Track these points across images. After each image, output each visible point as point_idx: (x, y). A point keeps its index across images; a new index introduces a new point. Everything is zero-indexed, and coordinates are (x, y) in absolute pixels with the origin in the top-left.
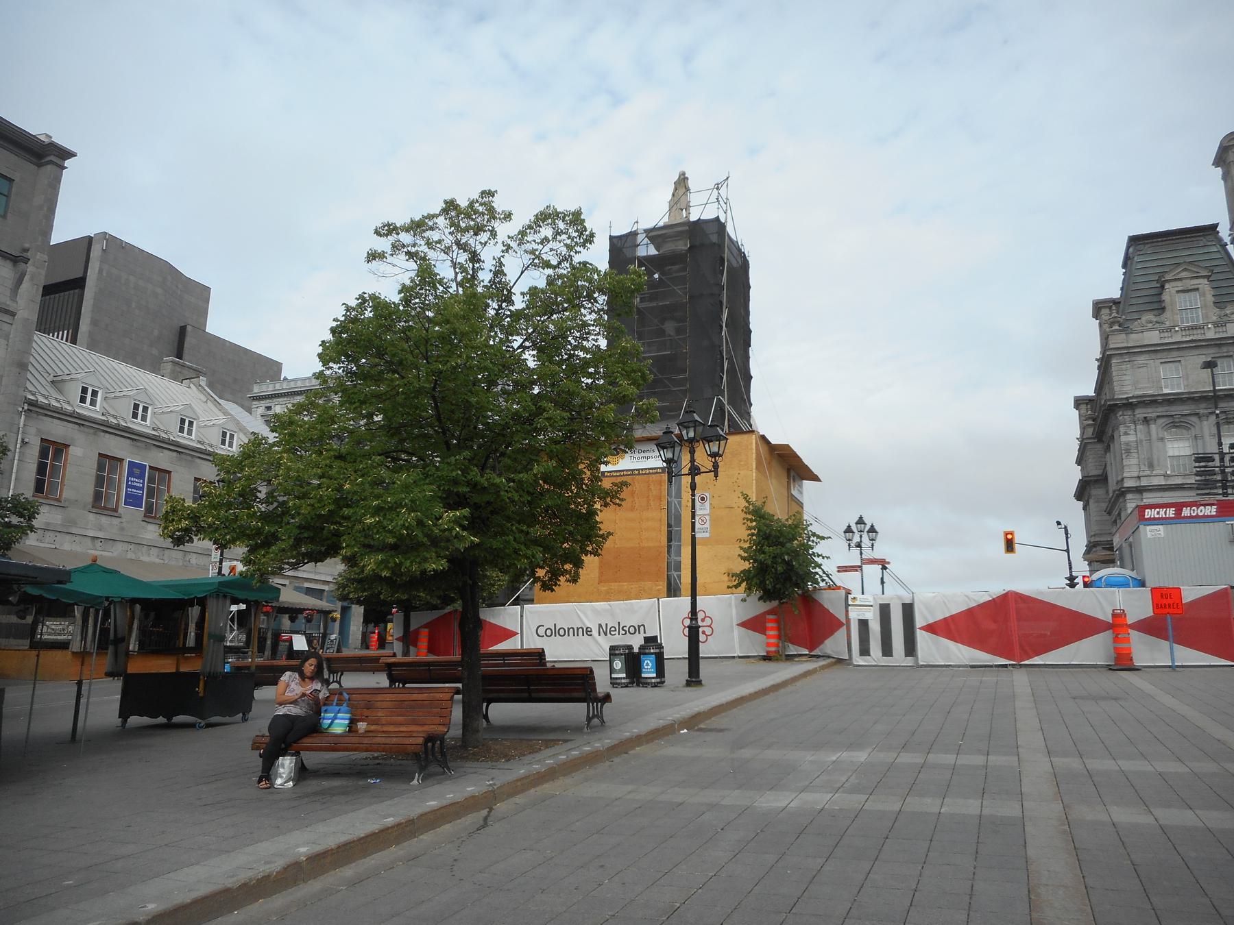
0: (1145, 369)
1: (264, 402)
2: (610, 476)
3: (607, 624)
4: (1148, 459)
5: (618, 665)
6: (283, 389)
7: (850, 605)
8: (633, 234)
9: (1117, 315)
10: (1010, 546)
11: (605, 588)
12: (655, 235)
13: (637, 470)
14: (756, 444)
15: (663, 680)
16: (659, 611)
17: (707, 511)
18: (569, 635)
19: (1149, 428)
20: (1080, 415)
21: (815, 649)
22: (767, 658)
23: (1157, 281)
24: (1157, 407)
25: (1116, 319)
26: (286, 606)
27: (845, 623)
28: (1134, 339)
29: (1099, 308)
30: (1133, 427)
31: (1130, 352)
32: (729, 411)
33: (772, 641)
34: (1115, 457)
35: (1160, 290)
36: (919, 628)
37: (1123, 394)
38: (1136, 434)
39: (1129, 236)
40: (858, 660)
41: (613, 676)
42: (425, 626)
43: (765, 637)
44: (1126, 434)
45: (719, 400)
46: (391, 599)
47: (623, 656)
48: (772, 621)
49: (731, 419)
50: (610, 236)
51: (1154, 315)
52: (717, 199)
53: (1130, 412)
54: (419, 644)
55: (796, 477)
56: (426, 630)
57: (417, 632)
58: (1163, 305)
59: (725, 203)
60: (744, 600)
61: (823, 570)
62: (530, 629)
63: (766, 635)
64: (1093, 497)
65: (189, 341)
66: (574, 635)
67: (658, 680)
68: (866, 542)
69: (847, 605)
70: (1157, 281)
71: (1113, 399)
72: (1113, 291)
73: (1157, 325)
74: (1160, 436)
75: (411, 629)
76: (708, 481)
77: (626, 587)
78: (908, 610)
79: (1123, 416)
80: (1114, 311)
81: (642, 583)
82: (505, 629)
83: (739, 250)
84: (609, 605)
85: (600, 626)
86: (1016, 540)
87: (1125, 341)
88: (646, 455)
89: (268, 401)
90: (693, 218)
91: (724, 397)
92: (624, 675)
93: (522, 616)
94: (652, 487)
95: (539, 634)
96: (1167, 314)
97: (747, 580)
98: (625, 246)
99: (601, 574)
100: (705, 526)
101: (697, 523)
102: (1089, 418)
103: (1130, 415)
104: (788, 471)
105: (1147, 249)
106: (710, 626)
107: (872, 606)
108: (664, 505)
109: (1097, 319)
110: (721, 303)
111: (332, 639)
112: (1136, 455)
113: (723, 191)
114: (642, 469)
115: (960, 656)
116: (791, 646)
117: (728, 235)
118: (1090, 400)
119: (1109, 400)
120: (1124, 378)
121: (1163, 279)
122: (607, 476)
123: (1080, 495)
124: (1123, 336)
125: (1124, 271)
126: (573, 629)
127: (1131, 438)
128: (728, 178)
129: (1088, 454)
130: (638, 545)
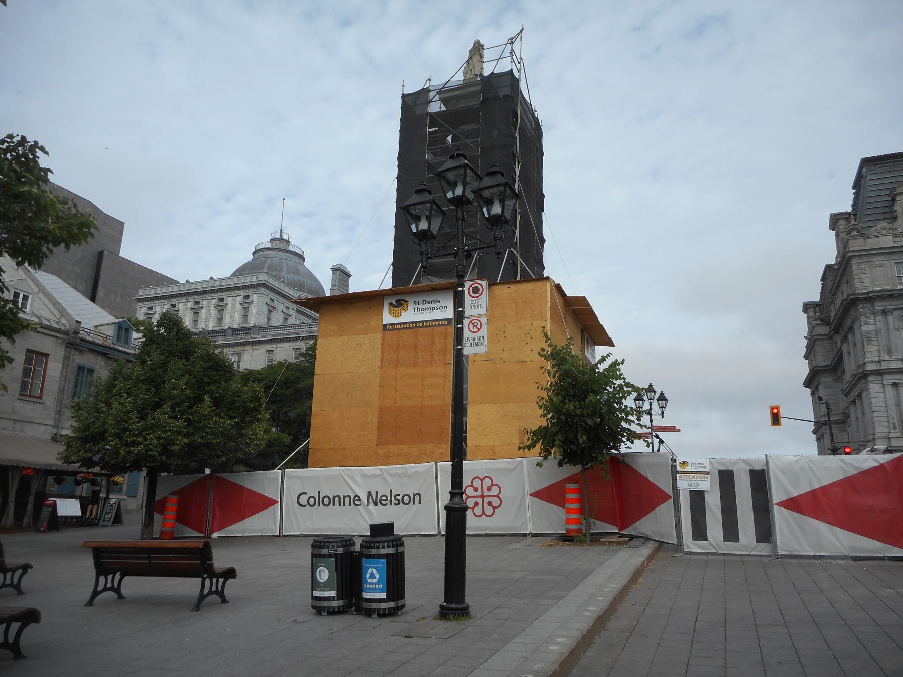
0: (881, 269)
1: (147, 303)
3: (377, 493)
4: (887, 346)
5: (323, 575)
6: (162, 293)
7: (678, 472)
8: (425, 91)
9: (855, 223)
10: (776, 419)
12: (448, 94)
14: (552, 295)
15: (401, 603)
16: (437, 478)
17: (483, 310)
18: (334, 505)
19: (887, 319)
20: (808, 318)
21: (625, 529)
22: (566, 538)
23: (889, 195)
24: (893, 301)
25: (854, 227)
26: (54, 469)
27: (672, 495)
28: (871, 243)
29: (835, 220)
30: (872, 318)
31: (869, 254)
32: (521, 264)
33: (573, 516)
34: (855, 344)
35: (891, 202)
36: (777, 504)
38: (876, 325)
40: (691, 545)
41: (317, 594)
42: (173, 494)
43: (564, 510)
44: (866, 324)
45: (511, 253)
46: (116, 461)
47: (333, 559)
48: (572, 491)
49: (523, 270)
50: (403, 94)
51: (887, 222)
52: (510, 53)
53: (869, 305)
54: (166, 513)
55: (589, 339)
56: (175, 497)
57: (164, 500)
59: (519, 63)
60: (539, 465)
62: (291, 497)
63: (565, 508)
64: (822, 384)
65: (105, 263)
66: (340, 505)
67: (392, 605)
68: (656, 409)
69: (674, 472)
70: (889, 195)
72: (847, 207)
73: (891, 231)
74: (897, 325)
75: (157, 499)
76: (498, 333)
78: (759, 479)
79: (863, 309)
80: (853, 220)
83: (533, 115)
84: (380, 469)
85: (369, 494)
86: (782, 414)
87: (864, 245)
88: (431, 306)
89: (150, 303)
90: (486, 73)
91: (516, 249)
92: (333, 594)
93: (283, 482)
94: (437, 341)
95: (478, 479)
96: (899, 222)
97: (544, 438)
99: (380, 435)
100: (479, 334)
101: (465, 330)
102: (817, 319)
103: (870, 308)
104: (583, 331)
105: (878, 169)
106: (497, 496)
107: (708, 473)
108: (450, 360)
109: (833, 230)
110: (514, 156)
111: (111, 503)
112: (876, 343)
113: (516, 46)
114: (426, 322)
115: (839, 544)
116: (597, 522)
117: (522, 94)
118: (817, 305)
119: (852, 295)
120: (863, 276)
121: (895, 192)
122: (390, 330)
123: (807, 384)
124: (862, 240)
125: (855, 190)
127: (871, 328)
128: (522, 30)
129: (817, 348)
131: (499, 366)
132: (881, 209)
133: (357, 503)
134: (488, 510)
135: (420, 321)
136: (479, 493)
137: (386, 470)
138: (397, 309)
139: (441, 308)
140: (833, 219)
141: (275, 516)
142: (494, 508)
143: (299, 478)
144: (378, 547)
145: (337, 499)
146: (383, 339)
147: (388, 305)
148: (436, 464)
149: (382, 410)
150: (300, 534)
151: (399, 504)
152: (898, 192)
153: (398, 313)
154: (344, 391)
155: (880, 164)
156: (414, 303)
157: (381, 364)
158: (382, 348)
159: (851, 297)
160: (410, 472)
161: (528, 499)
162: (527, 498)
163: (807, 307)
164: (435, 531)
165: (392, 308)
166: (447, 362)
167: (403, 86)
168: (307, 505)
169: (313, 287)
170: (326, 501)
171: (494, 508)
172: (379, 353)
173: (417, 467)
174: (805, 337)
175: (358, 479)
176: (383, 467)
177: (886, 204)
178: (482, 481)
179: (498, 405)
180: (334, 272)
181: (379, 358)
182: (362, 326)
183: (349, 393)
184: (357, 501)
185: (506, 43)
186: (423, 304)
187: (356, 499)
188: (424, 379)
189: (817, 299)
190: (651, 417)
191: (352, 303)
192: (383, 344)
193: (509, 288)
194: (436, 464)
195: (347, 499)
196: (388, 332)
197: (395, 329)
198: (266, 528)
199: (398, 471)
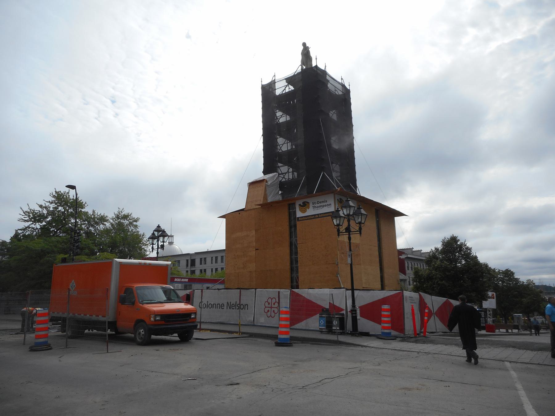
3: (230, 302)
18: (245, 309)
61: (398, 282)
66: (215, 308)
88: (322, 204)
114: (320, 214)
126: (205, 304)
135: (316, 214)
138: (304, 208)
142: (267, 302)
144: (340, 332)
147: (298, 206)
170: (210, 306)
171: (267, 302)
190: (349, 235)
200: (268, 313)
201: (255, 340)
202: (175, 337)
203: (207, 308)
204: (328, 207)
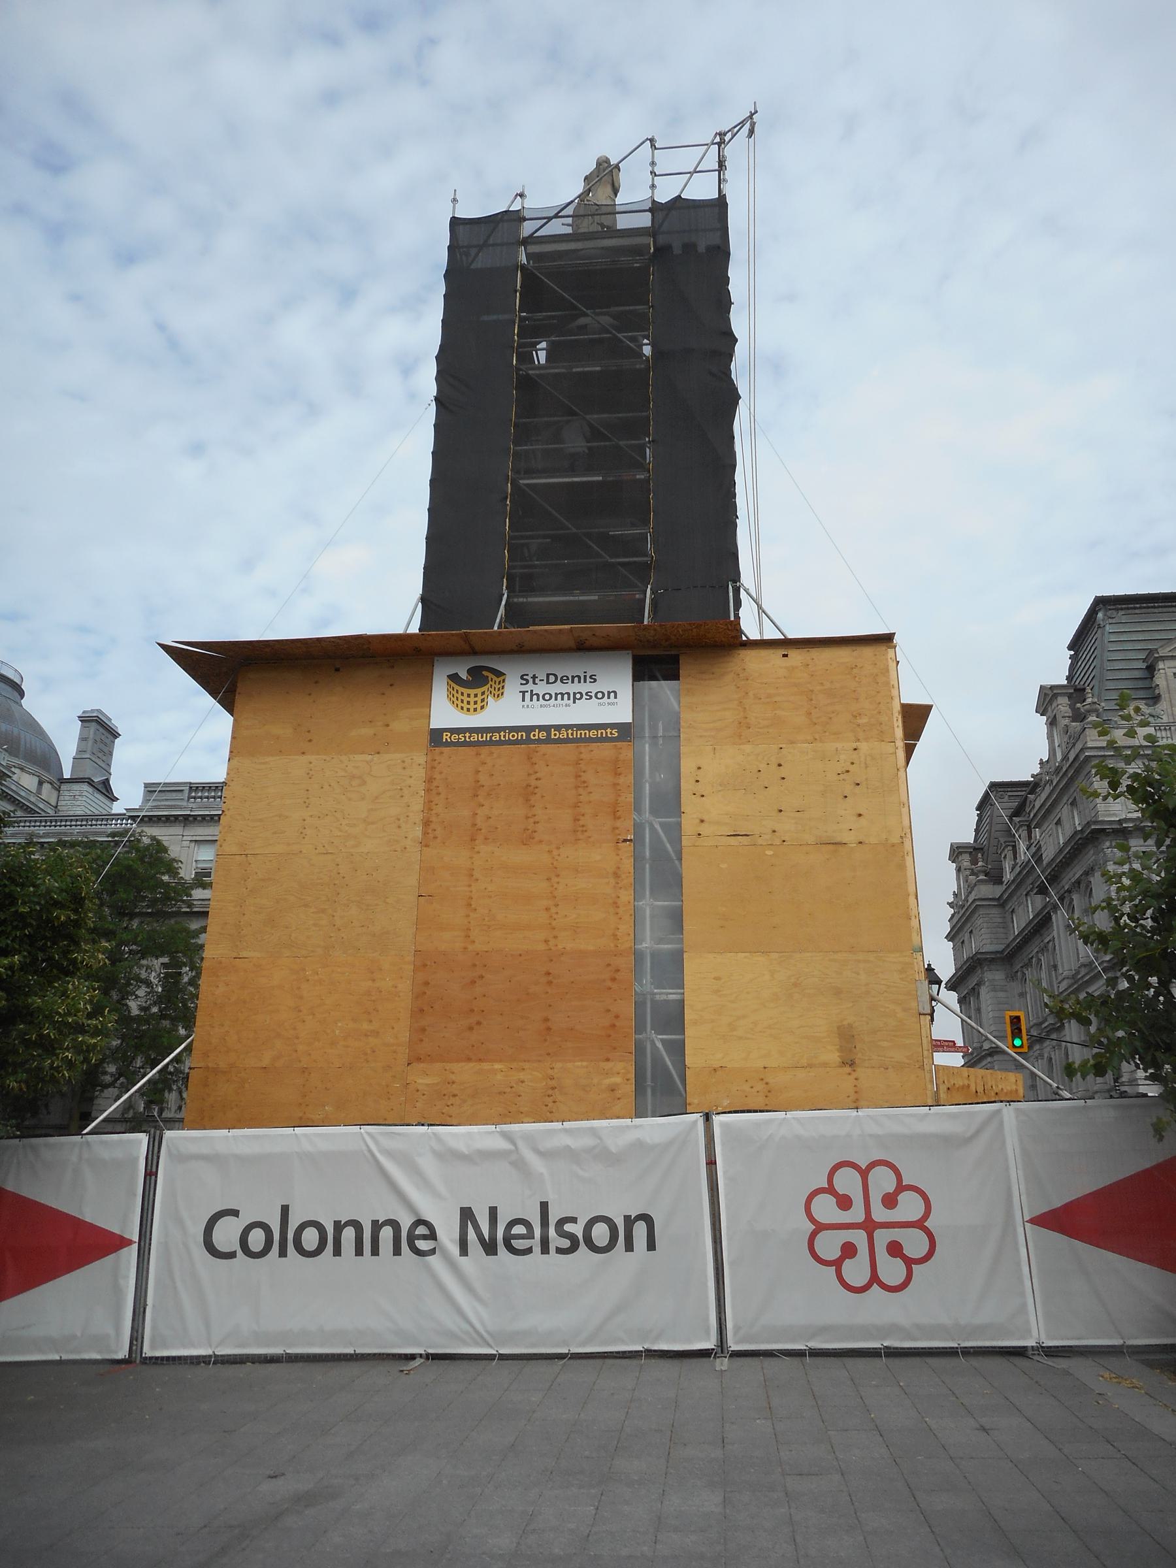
2: (458, 744)
3: (493, 1212)
11: (428, 1081)
13: (541, 728)
16: (711, 1163)
23: (1144, 660)
37: (1110, 815)
39: (1096, 596)
58: (1157, 692)
64: (987, 984)
66: (359, 1252)
70: (1144, 660)
71: (1096, 822)
76: (762, 766)
77: (499, 1077)
81: (558, 1065)
82: (77, 1224)
85: (467, 1215)
93: (151, 1174)
96: (1163, 705)
98: (491, 241)
105: (1121, 616)
106: (920, 1224)
114: (558, 728)
121: (1156, 655)
125: (1072, 653)
130: (542, 947)
131: (769, 853)
132: (1126, 682)
133: (422, 1245)
134: (892, 1271)
136: (857, 1214)
137: (529, 1138)
138: (472, 692)
139: (600, 695)
140: (1046, 694)
141: (118, 1291)
143: (214, 1159)
145: (349, 1234)
146: (431, 767)
147: (445, 680)
148: (707, 1117)
149: (424, 962)
150: (210, 1353)
151: (574, 1248)
152: (1161, 655)
153: (476, 703)
154: (306, 906)
155: (1125, 609)
156: (522, 678)
157: (425, 833)
158: (428, 791)
159: (1093, 827)
160: (615, 1144)
161: (1024, 1233)
162: (1020, 1230)
163: (957, 852)
164: (708, 1339)
165: (456, 687)
166: (622, 838)
167: (455, 200)
168: (240, 1253)
169: (38, 750)
170: (310, 1238)
171: (909, 1262)
172: (417, 805)
173: (636, 1127)
174: (948, 903)
175: (429, 1165)
176: (515, 1127)
177: (1137, 674)
178: (864, 1173)
179: (774, 956)
180: (87, 724)
181: (418, 818)
182: (367, 731)
183: (323, 911)
184: (424, 1237)
185: (709, 141)
186: (548, 682)
187: (421, 1230)
188: (555, 880)
189: (968, 837)
191: (337, 670)
192: (429, 780)
193: (785, 656)
194: (707, 1117)
195: (387, 1233)
196: (446, 750)
197: (465, 744)
198: (79, 1334)
199: (568, 1141)
200: (847, 1265)
201: (1094, 659)
202: (905, 810)
203: (283, 1253)
204: (600, 704)
